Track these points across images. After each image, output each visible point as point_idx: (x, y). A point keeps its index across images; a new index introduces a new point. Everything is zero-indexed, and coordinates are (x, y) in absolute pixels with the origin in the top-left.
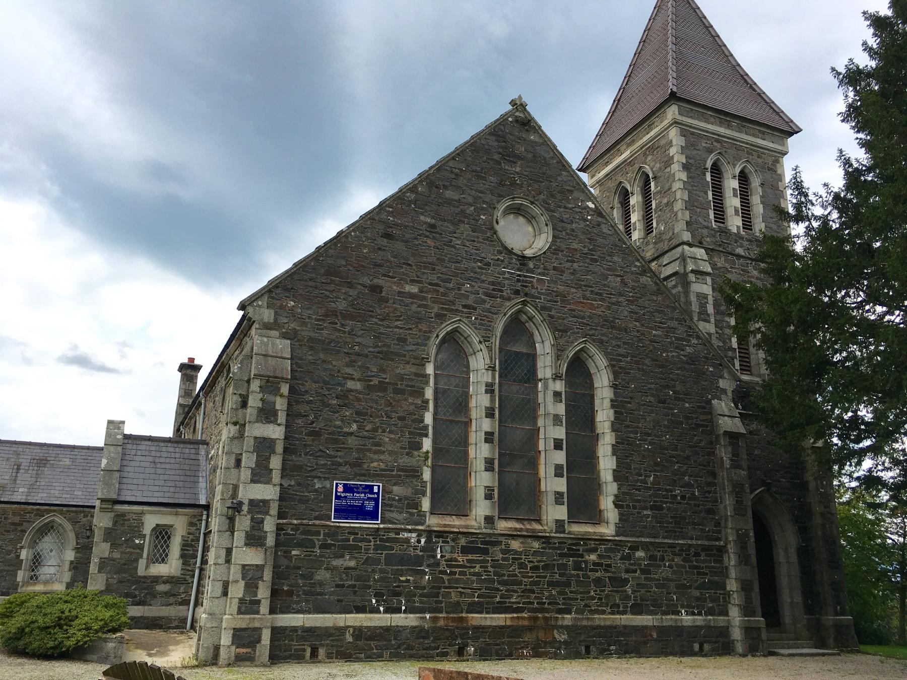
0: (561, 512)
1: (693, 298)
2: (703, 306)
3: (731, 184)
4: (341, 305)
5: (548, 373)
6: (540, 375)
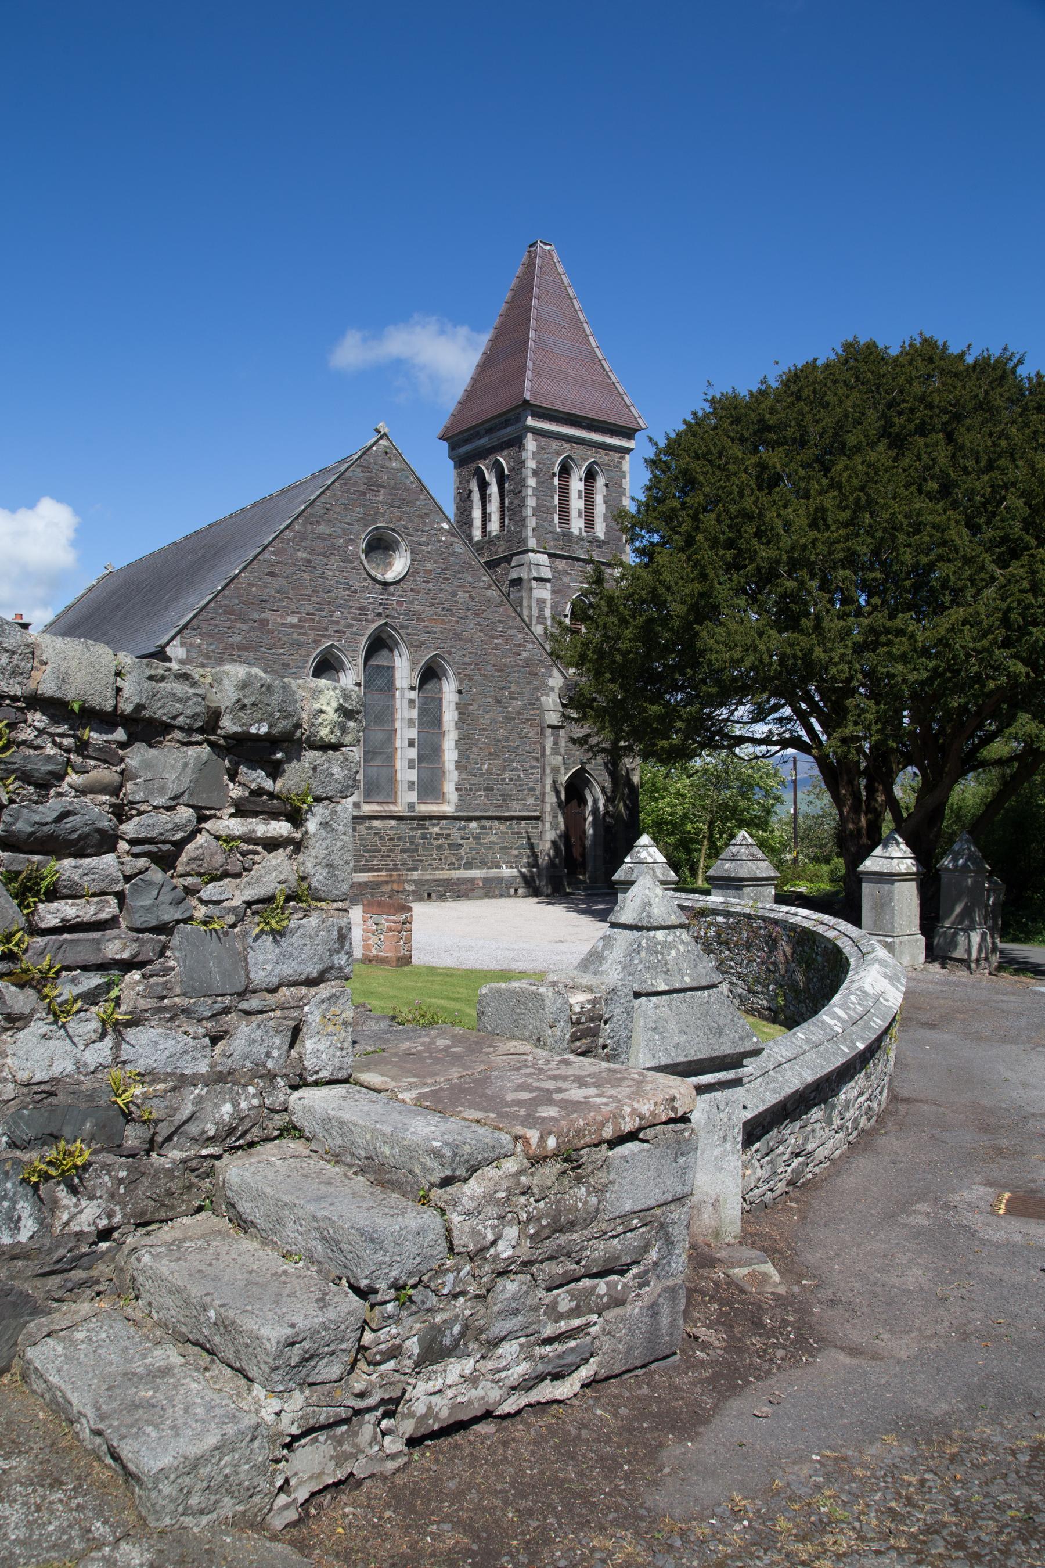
0: (413, 797)
1: (534, 605)
2: (541, 610)
3: (576, 485)
4: (238, 639)
6: (398, 684)
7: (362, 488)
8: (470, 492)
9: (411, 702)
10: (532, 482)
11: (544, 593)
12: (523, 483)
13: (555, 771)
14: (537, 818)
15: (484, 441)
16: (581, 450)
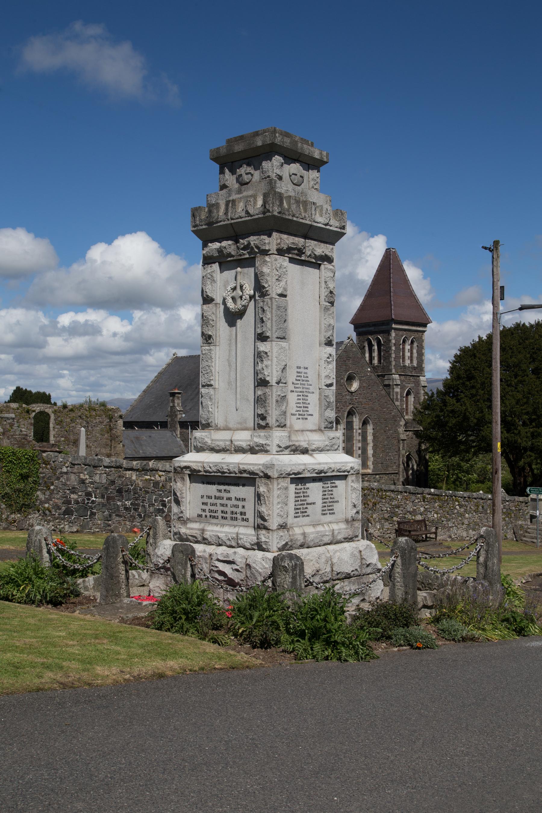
1: (395, 394)
2: (397, 396)
3: (407, 347)
5: (357, 428)
6: (355, 427)
7: (345, 359)
8: (364, 346)
9: (359, 433)
10: (393, 348)
11: (397, 390)
12: (390, 348)
13: (403, 456)
14: (397, 473)
15: (372, 329)
16: (409, 333)
